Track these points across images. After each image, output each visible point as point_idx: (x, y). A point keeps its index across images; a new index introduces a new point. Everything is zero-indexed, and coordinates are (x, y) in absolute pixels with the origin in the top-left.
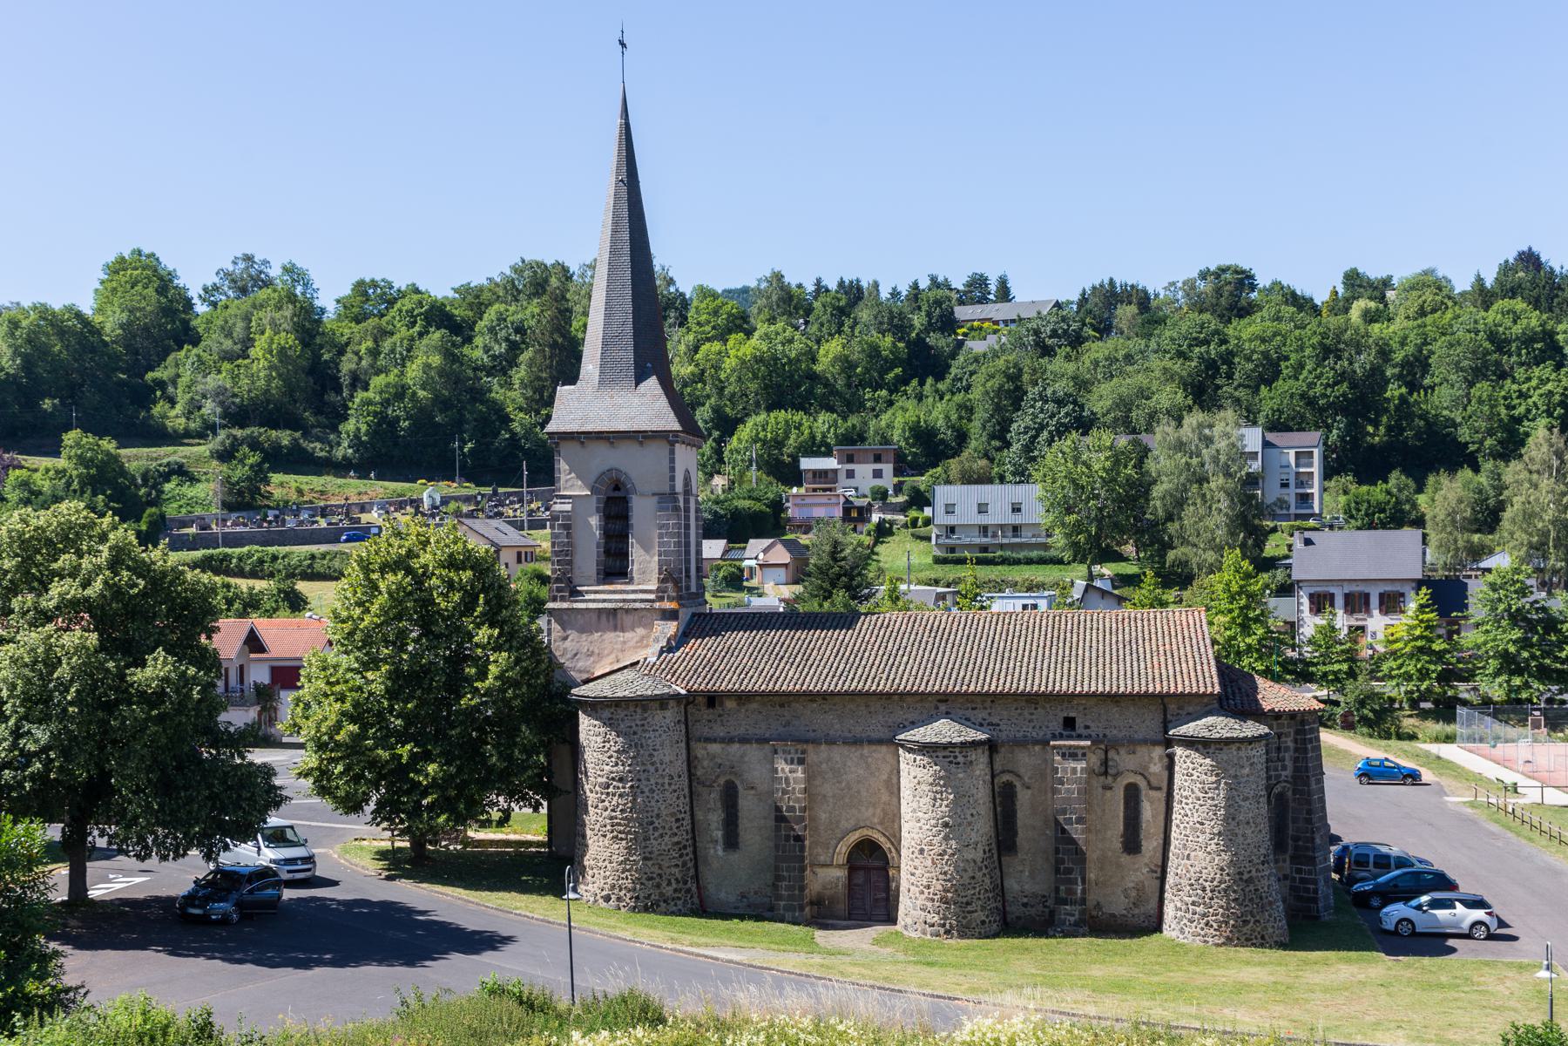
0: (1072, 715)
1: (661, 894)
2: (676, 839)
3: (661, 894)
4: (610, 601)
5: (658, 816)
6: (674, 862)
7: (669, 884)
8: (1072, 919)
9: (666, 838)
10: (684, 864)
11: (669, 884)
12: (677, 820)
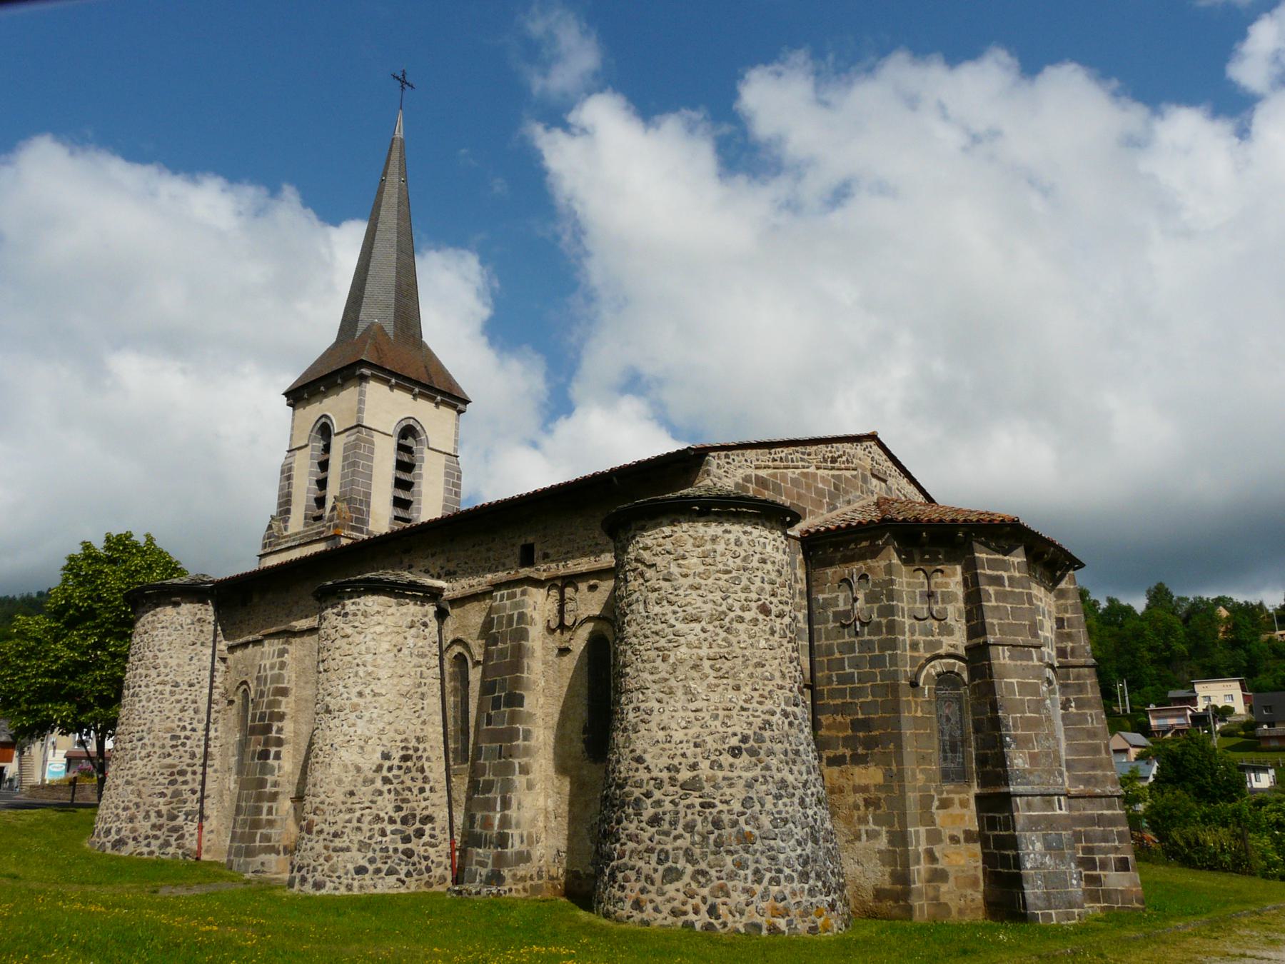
0: (530, 540)
1: (134, 830)
2: (168, 761)
3: (134, 830)
5: (150, 731)
6: (160, 789)
7: (147, 816)
8: (484, 871)
9: (155, 758)
10: (176, 794)
11: (147, 816)
12: (174, 737)
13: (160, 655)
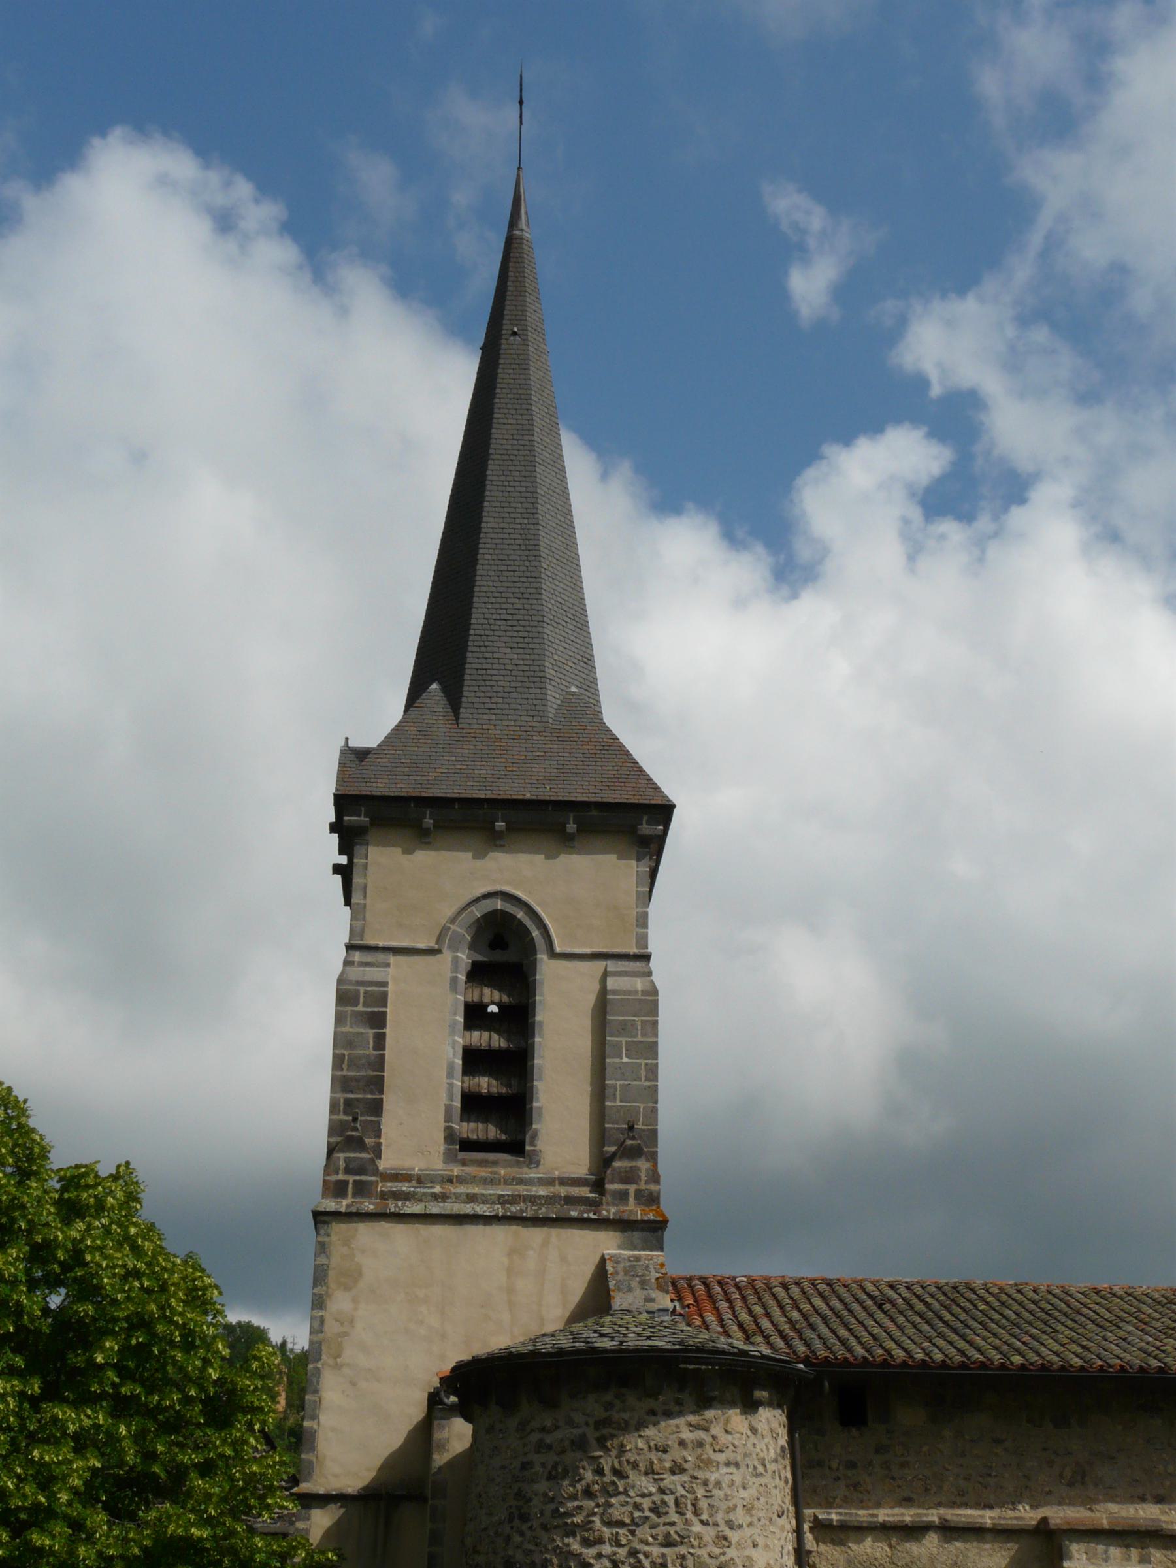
4: (485, 1200)
13: (734, 1536)
